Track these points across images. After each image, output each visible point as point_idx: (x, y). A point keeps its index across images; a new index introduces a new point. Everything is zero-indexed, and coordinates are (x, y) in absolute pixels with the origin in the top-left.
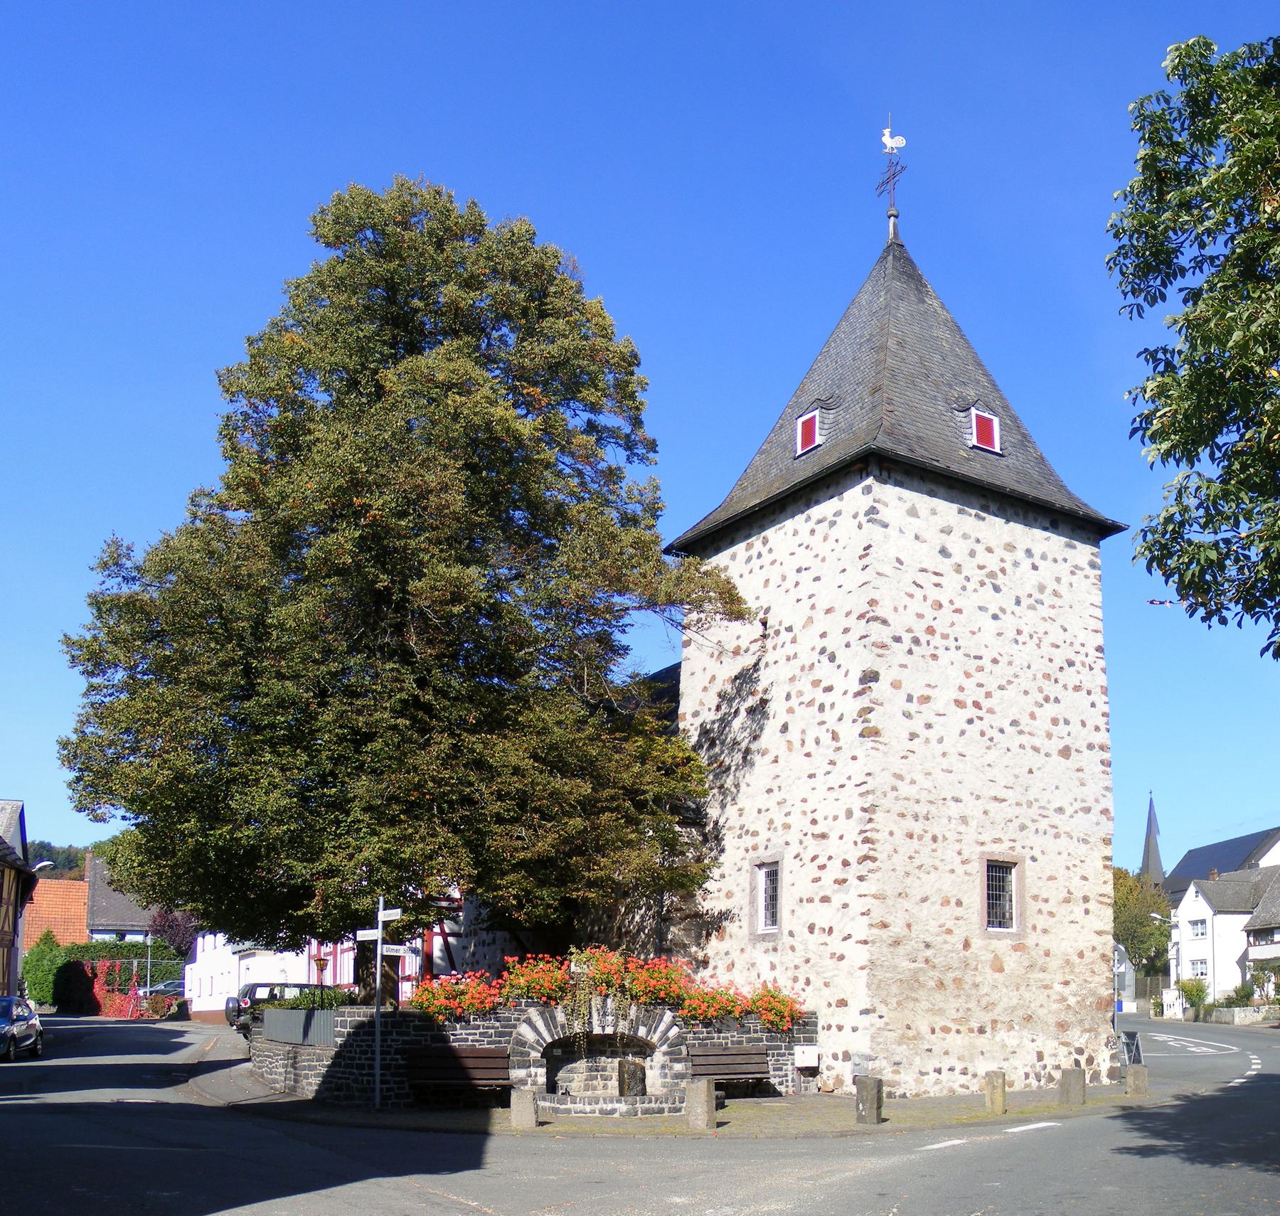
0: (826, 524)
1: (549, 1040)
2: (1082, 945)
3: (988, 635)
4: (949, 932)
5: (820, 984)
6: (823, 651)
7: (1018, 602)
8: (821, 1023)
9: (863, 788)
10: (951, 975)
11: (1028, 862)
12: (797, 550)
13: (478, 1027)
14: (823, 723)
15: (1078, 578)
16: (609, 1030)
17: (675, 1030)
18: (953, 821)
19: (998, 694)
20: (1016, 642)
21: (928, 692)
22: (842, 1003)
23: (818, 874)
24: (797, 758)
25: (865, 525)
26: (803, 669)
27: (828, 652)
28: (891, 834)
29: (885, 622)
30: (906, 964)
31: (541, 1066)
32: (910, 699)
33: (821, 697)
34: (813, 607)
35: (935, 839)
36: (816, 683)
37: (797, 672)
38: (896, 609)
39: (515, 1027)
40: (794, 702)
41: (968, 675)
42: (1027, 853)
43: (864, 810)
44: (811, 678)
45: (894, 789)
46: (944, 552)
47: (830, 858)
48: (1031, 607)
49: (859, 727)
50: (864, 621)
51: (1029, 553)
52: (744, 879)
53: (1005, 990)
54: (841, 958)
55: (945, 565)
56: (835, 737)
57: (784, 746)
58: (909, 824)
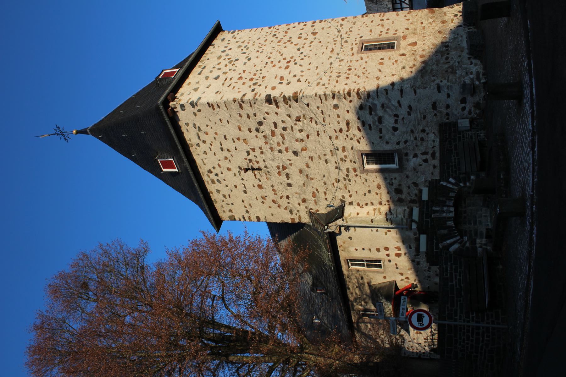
0: (200, 133)
2: (404, 19)
6: (257, 130)
7: (244, 53)
8: (445, 120)
9: (323, 98)
11: (362, 39)
12: (213, 151)
14: (292, 127)
15: (238, 37)
16: (452, 209)
17: (451, 180)
21: (279, 77)
24: (310, 145)
25: (199, 108)
26: (266, 143)
27: (258, 126)
28: (346, 84)
32: (281, 83)
33: (279, 131)
35: (350, 70)
36: (273, 134)
38: (239, 92)
41: (274, 66)
42: (358, 39)
45: (324, 85)
46: (217, 78)
48: (247, 49)
50: (243, 105)
51: (224, 51)
54: (410, 107)
55: (223, 77)
56: (298, 119)
57: (304, 152)
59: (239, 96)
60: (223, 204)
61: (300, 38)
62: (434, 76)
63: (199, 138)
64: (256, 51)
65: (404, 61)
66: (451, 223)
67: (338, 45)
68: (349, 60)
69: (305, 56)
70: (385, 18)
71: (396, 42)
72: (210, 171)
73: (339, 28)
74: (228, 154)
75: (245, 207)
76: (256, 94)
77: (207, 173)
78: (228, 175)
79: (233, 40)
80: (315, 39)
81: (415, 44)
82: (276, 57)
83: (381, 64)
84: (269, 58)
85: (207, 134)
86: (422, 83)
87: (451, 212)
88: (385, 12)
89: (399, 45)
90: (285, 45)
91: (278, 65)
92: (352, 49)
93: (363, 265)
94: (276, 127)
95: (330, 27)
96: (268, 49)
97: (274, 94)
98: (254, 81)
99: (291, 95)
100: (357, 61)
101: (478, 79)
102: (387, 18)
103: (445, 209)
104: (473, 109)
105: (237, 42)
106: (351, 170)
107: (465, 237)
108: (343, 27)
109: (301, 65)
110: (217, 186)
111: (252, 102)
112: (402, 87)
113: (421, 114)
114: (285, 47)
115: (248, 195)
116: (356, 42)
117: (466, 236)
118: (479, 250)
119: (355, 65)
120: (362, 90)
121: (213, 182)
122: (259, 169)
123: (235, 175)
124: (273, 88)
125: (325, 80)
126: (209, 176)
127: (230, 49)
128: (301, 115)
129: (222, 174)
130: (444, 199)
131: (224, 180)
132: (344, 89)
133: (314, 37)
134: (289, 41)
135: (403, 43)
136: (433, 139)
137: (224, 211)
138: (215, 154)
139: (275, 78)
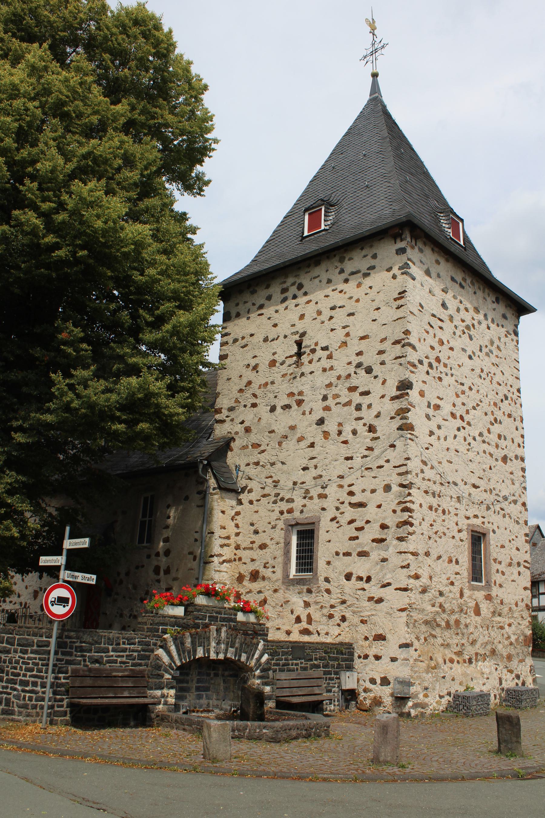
0: (360, 275)
1: (179, 664)
2: (518, 598)
3: (466, 370)
4: (452, 584)
5: (356, 620)
6: (359, 365)
7: (481, 350)
9: (403, 469)
10: (454, 617)
11: (491, 533)
13: (124, 650)
16: (221, 656)
17: (266, 657)
18: (453, 499)
19: (472, 412)
20: (481, 377)
21: (438, 402)
22: (380, 638)
23: (355, 534)
28: (421, 505)
29: (414, 348)
30: (429, 608)
31: (172, 688)
32: (429, 406)
33: (356, 398)
34: (348, 335)
35: (444, 512)
36: (352, 389)
37: (334, 380)
38: (420, 340)
39: (152, 651)
40: (330, 402)
41: (458, 396)
43: (402, 486)
44: (348, 385)
45: (422, 471)
46: (444, 305)
47: (368, 522)
48: (487, 355)
49: (398, 422)
52: (279, 535)
53: (481, 629)
54: (380, 601)
55: (443, 314)
58: (430, 499)
61: (500, 437)
62: (426, 639)
63: (353, 273)
65: (451, 595)
66: (200, 653)
68: (458, 512)
69: (469, 444)
70: (522, 569)
73: (511, 498)
77: (298, 281)
81: (477, 612)
82: (471, 399)
83: (450, 561)
86: (415, 621)
87: (217, 654)
90: (489, 413)
92: (476, 516)
93: (144, 516)
96: (484, 386)
98: (435, 364)
100: (457, 524)
101: (415, 706)
105: (499, 339)
106: (290, 505)
108: (513, 504)
109: (455, 437)
113: (369, 616)
114: (486, 414)
116: (486, 523)
117: (181, 674)
118: (158, 693)
121: (284, 291)
123: (293, 325)
124: (422, 394)
125: (429, 473)
129: (296, 306)
130: (237, 645)
131: (286, 308)
132: (413, 503)
133: (500, 459)
134: (496, 420)
135: (480, 595)
136: (329, 633)
137: (237, 305)
139: (438, 398)
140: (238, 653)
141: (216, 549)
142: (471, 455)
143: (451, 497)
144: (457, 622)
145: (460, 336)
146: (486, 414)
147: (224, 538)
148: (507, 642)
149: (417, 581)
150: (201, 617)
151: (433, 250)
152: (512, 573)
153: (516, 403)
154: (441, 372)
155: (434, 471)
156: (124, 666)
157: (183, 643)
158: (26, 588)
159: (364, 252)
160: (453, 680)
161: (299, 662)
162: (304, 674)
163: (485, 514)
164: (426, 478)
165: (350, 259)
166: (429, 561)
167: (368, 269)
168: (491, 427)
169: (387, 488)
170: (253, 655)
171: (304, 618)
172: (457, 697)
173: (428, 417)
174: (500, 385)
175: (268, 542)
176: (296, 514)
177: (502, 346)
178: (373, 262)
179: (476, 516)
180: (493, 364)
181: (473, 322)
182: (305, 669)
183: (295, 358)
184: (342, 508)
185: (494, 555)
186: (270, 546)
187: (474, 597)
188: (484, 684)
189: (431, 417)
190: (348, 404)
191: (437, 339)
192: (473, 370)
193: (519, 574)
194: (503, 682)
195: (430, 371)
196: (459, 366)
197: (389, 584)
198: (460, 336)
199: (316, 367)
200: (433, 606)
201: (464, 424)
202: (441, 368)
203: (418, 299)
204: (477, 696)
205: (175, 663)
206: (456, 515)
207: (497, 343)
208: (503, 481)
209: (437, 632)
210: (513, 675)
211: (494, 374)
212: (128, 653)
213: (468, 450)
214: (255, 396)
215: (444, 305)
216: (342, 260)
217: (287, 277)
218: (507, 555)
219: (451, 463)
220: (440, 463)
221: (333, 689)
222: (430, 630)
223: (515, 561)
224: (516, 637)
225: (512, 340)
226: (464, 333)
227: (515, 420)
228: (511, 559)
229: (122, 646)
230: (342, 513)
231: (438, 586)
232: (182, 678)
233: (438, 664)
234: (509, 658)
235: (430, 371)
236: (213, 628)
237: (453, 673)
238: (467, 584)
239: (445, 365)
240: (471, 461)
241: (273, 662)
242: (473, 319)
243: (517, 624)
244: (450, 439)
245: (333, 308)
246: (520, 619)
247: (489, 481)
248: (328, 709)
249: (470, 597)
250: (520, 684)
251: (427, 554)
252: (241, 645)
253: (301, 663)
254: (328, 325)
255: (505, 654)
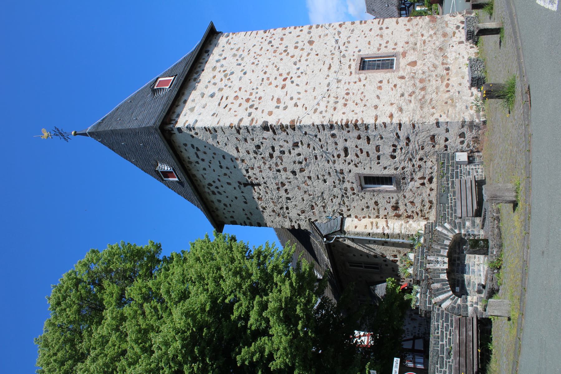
0: (198, 153)
1: (451, 293)
2: (404, 29)
3: (253, 77)
4: (395, 86)
5: (421, 152)
6: (255, 152)
7: (240, 65)
9: (321, 127)
11: (361, 53)
12: (212, 168)
13: (442, 332)
16: (446, 260)
17: (447, 225)
20: (257, 64)
21: (275, 99)
23: (365, 153)
28: (344, 113)
29: (241, 120)
30: (412, 105)
31: (466, 299)
32: (278, 107)
33: (277, 154)
35: (348, 94)
38: (236, 116)
40: (281, 167)
41: (270, 84)
42: (357, 54)
45: (321, 113)
46: (212, 96)
47: (357, 147)
48: (242, 59)
53: (426, 60)
55: (218, 95)
58: (339, 106)
59: (235, 123)
60: (224, 211)
61: (296, 47)
62: (433, 108)
63: (198, 157)
64: (251, 62)
65: (403, 86)
66: (444, 276)
67: (336, 61)
68: (347, 81)
69: (302, 73)
70: (384, 26)
71: (395, 58)
72: (210, 185)
73: (337, 37)
74: (228, 172)
75: (246, 214)
76: (252, 120)
77: (207, 186)
78: (229, 189)
79: (227, 47)
80: (311, 50)
81: (414, 64)
82: (272, 72)
83: (380, 88)
84: (265, 73)
85: (205, 153)
86: (421, 117)
87: (445, 263)
88: (384, 18)
89: (398, 64)
90: (281, 56)
91: (275, 83)
92: (350, 67)
93: (362, 267)
94: (274, 151)
95: (327, 35)
96: (263, 61)
97: (272, 121)
98: (251, 103)
99: (289, 124)
100: (355, 82)
102: (386, 26)
103: (440, 259)
104: (472, 143)
105: (232, 49)
106: (349, 190)
107: (457, 288)
108: (341, 35)
109: (297, 85)
110: (218, 197)
111: (250, 129)
112: (400, 120)
113: (419, 146)
114: (281, 59)
115: (248, 205)
116: (354, 58)
117: (458, 286)
118: (470, 309)
119: (354, 88)
120: (360, 122)
121: (214, 193)
122: (259, 185)
123: (235, 188)
124: (270, 113)
125: (322, 108)
126: (209, 188)
127: (225, 58)
128: (299, 141)
129: (222, 186)
130: (439, 248)
131: (225, 192)
133: (311, 47)
134: (285, 51)
135: (403, 62)
137: (226, 217)
138: (214, 171)
139: (272, 99)
140: (444, 247)
141: (380, 231)
142: (309, 72)
143: (337, 87)
144: (422, 81)
145: (232, 82)
146: (281, 59)
147: (372, 226)
148: (434, 38)
149: (394, 116)
150: (421, 275)
151: (177, 106)
152: (387, 34)
153: (274, 34)
154: (256, 98)
155: (321, 103)
156: (452, 333)
157: (438, 290)
158: (409, 324)
159: (183, 151)
160: (460, 84)
161: (450, 198)
162: (458, 195)
163: (347, 58)
164: (326, 109)
165: (189, 158)
166: (380, 106)
167: (194, 148)
168: (290, 55)
169: (333, 136)
170: (445, 235)
171: (422, 181)
172: (472, 85)
173: (285, 108)
174: (262, 48)
175: (373, 201)
176: (355, 186)
177: (237, 47)
178: (189, 146)
179: (350, 67)
180: (248, 54)
181: (222, 71)
182: (454, 193)
183: (255, 187)
184: (348, 161)
185: (375, 50)
186: (376, 200)
187: (404, 67)
188: (463, 57)
189: (285, 105)
190: (281, 158)
191: (234, 101)
192: (253, 71)
193: (387, 28)
194: (461, 40)
195: (255, 107)
196: (251, 82)
197: (397, 134)
198: (232, 82)
199: (258, 174)
200: (410, 101)
201: (289, 77)
202: (252, 98)
203: (209, 117)
204: (471, 70)
205: (451, 296)
206: (349, 83)
207: (234, 51)
208: (326, 44)
209: (428, 97)
210: (457, 31)
211: (255, 53)
212: (444, 330)
213: (306, 74)
214: (282, 208)
215: (212, 96)
216: (190, 163)
217: (205, 192)
218: (375, 39)
219: (315, 88)
220: (315, 98)
221: (468, 170)
222: (427, 103)
223: (379, 32)
224: (430, 29)
225: (232, 38)
226: (229, 79)
227: (284, 35)
228: (377, 35)
229: (439, 334)
230: (352, 161)
231: (397, 98)
232: (460, 285)
233: (450, 98)
234: (445, 35)
235: (255, 107)
236: (428, 266)
237: (456, 85)
238: (395, 73)
239: (251, 94)
240: (313, 72)
241: (450, 218)
242: (220, 72)
243: (422, 29)
244: (299, 89)
245: (221, 167)
246: (418, 26)
247: (326, 56)
248: (481, 173)
249: (404, 70)
250: (463, 25)
251: (376, 107)
252: (439, 244)
253: (450, 196)
254: (232, 169)
255: (442, 39)
